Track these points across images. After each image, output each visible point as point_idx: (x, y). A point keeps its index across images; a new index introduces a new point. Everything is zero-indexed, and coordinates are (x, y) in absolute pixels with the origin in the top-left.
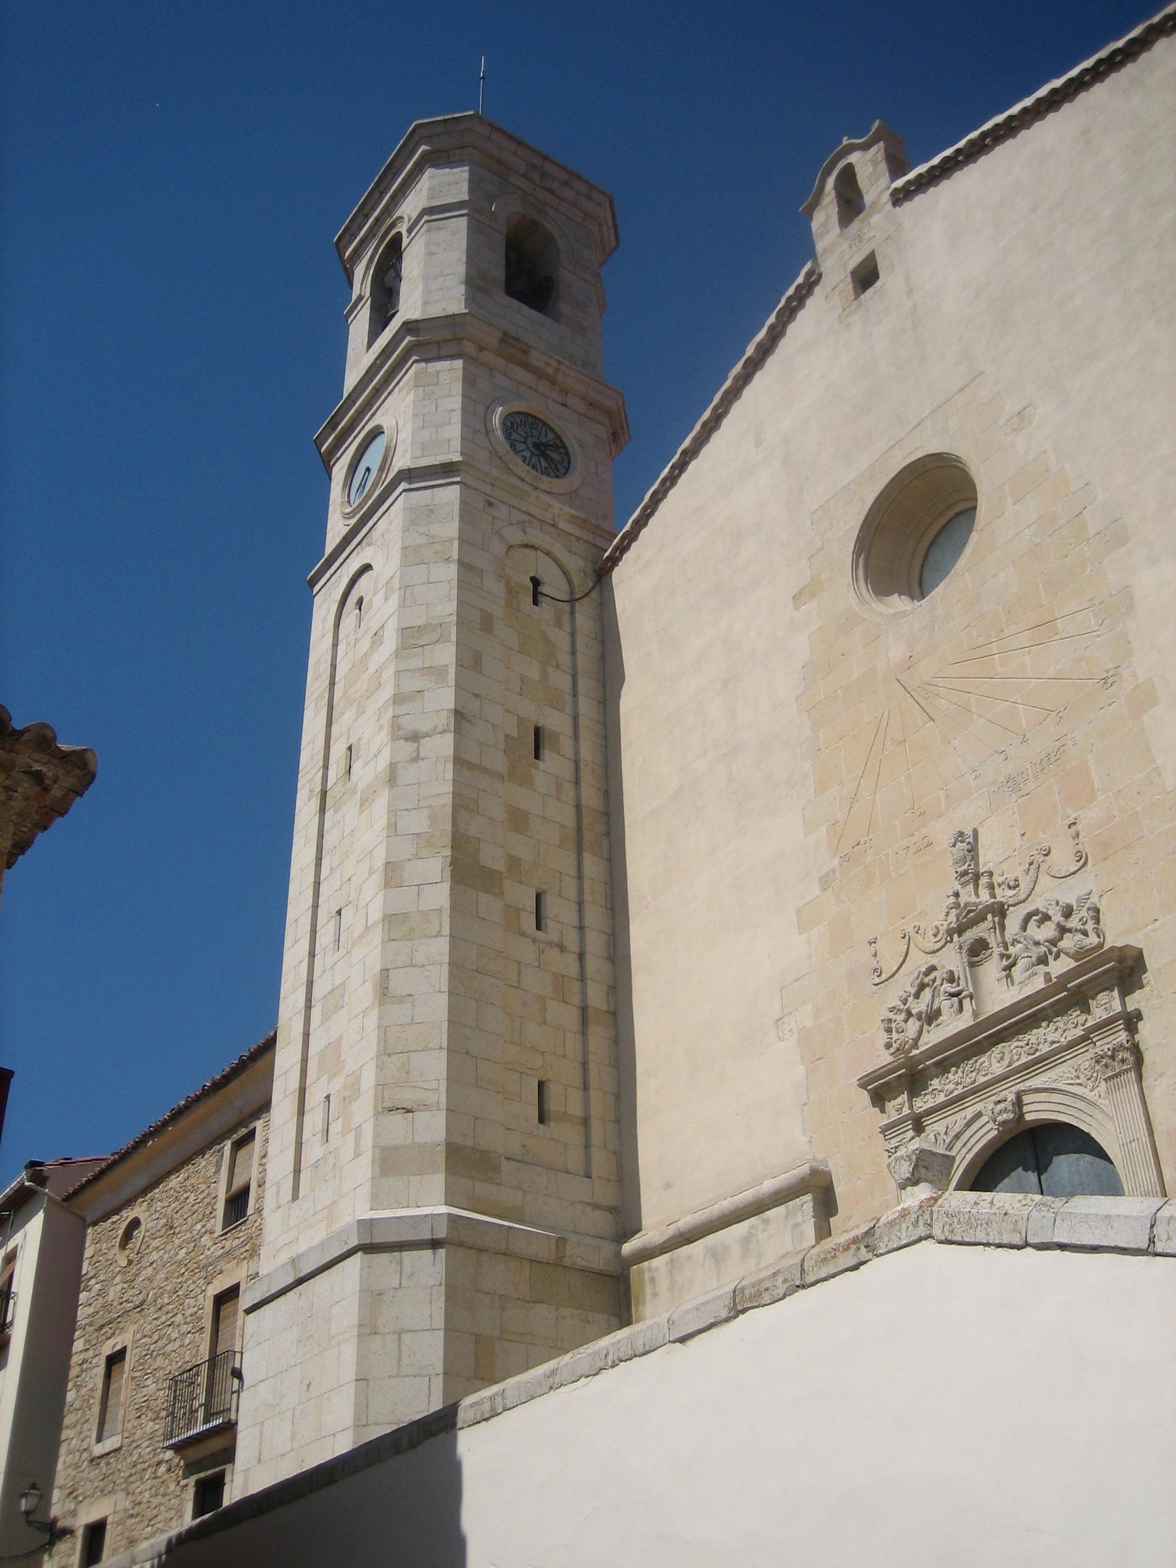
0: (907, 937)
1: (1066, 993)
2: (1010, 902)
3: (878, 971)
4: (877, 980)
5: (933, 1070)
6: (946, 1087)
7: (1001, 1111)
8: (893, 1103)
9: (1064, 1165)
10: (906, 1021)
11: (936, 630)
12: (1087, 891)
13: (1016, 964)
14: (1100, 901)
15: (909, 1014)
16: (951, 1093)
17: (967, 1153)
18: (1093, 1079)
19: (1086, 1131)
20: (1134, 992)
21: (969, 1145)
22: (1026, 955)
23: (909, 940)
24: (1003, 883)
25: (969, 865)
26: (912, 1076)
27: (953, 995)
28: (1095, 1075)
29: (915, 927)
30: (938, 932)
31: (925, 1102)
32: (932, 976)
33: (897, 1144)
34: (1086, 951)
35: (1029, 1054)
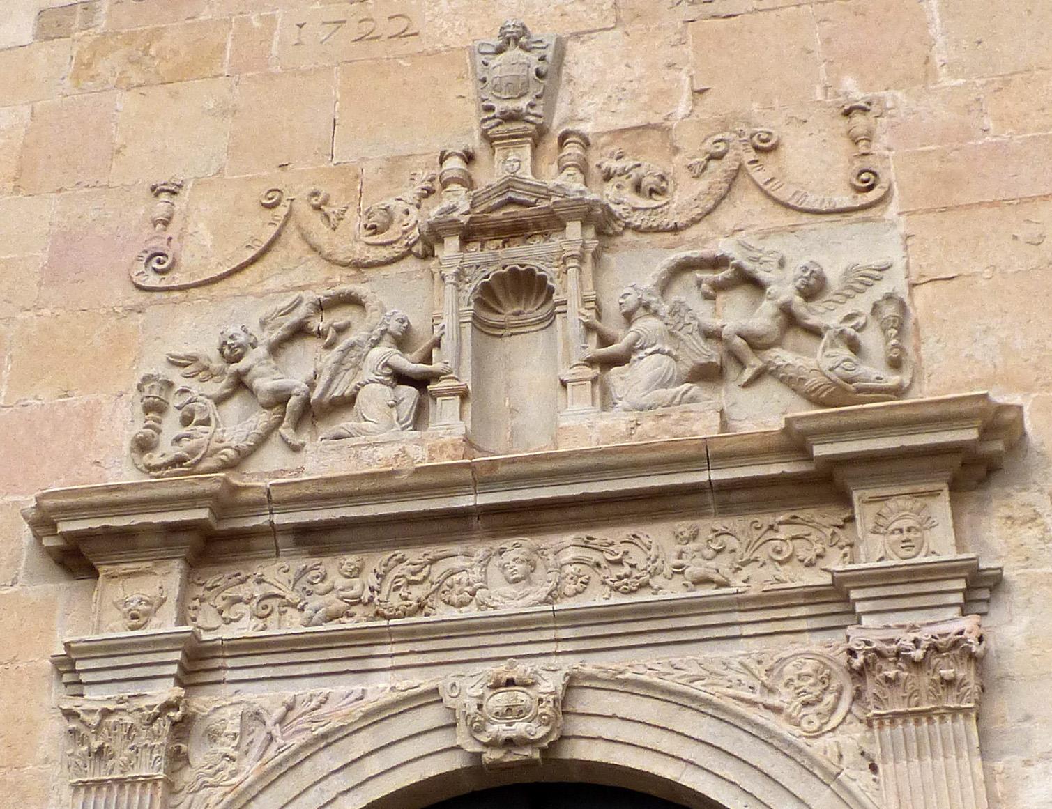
0: (282, 211)
2: (636, 220)
4: (153, 280)
6: (315, 602)
9: (67, 712)
10: (220, 400)
11: (163, 26)
12: (877, 262)
14: (910, 295)
15: (240, 384)
18: (819, 707)
22: (667, 349)
23: (288, 216)
25: (532, 106)
27: (400, 378)
28: (829, 698)
29: (315, 194)
30: (386, 227)
31: (228, 622)
32: (339, 317)
33: (111, 706)
34: (860, 390)
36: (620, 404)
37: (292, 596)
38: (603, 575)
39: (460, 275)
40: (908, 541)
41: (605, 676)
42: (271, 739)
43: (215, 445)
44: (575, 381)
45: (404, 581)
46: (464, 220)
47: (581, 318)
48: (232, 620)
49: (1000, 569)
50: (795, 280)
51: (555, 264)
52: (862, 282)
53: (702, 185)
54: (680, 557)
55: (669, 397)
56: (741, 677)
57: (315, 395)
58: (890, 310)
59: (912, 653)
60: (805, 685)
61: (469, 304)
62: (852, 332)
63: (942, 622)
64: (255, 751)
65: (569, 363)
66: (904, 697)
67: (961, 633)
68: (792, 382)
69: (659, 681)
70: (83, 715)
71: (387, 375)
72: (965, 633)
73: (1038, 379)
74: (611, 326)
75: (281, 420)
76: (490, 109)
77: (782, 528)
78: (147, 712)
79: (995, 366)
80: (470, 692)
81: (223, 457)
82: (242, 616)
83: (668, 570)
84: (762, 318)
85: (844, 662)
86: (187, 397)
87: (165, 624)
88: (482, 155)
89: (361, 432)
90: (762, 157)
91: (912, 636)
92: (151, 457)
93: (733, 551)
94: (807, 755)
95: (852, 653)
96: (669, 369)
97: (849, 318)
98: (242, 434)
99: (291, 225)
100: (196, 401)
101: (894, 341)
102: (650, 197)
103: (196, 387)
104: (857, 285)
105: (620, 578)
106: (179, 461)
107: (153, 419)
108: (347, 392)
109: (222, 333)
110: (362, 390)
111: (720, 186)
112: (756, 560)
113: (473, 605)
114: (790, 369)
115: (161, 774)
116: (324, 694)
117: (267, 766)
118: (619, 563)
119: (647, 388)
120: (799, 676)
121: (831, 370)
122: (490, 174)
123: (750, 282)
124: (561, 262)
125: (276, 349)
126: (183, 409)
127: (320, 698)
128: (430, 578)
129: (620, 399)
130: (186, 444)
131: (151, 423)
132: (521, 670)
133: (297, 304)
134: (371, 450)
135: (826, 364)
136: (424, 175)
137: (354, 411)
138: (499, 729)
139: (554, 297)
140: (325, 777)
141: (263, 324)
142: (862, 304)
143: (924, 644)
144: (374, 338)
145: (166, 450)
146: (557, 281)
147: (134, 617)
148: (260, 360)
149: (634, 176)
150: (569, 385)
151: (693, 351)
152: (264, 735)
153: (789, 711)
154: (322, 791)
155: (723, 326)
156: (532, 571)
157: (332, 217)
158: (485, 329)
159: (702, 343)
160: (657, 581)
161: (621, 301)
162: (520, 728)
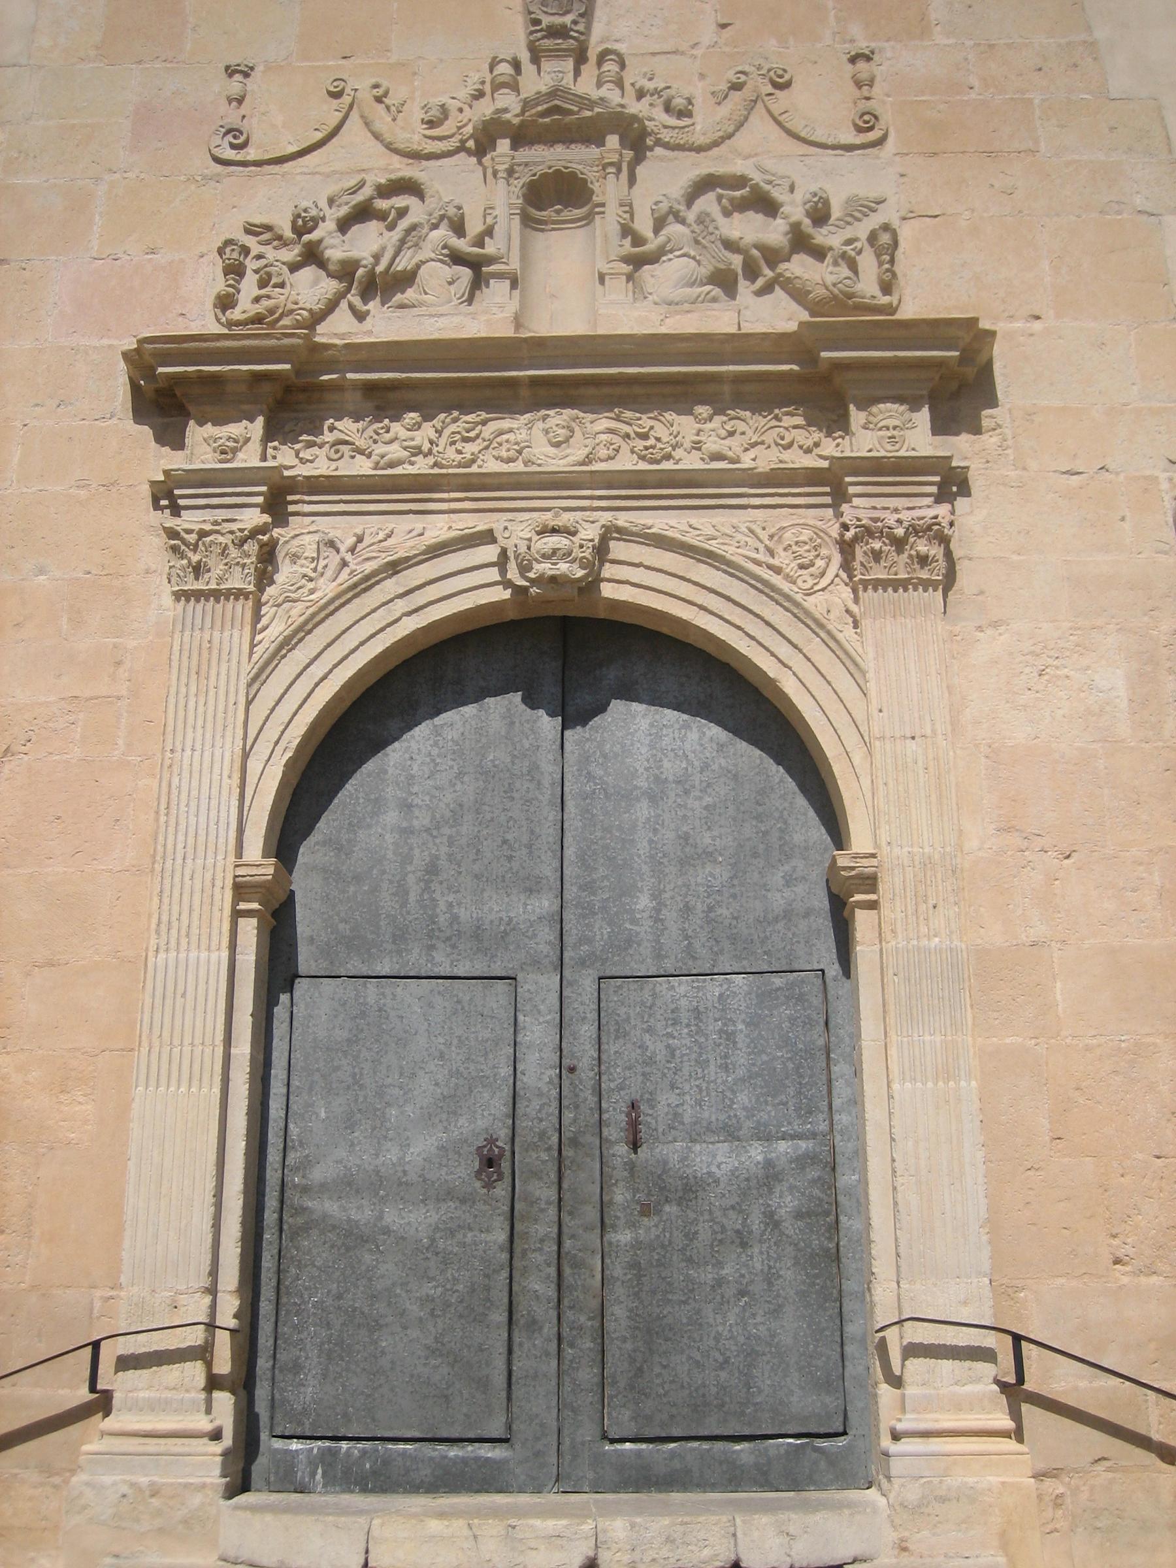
0: (346, 99)
1: (795, 367)
2: (666, 136)
3: (237, 137)
4: (230, 154)
5: (353, 399)
6: (380, 449)
7: (555, 551)
8: (209, 429)
10: (294, 267)
12: (873, 195)
13: (657, 261)
15: (313, 256)
16: (391, 465)
17: (409, 614)
19: (771, 675)
20: (957, 434)
21: (419, 598)
23: (351, 106)
24: (657, 92)
25: (575, 22)
26: (288, 389)
27: (457, 258)
29: (376, 86)
31: (303, 461)
32: (400, 201)
35: (643, 458)
36: (650, 297)
37: (361, 443)
38: (632, 444)
39: (510, 172)
40: (894, 437)
41: (634, 529)
42: (344, 564)
43: (291, 306)
44: (612, 274)
45: (458, 437)
46: (516, 121)
47: (620, 220)
48: (308, 461)
49: (968, 468)
50: (805, 204)
51: (595, 169)
52: (860, 211)
53: (724, 110)
54: (698, 435)
55: (695, 296)
56: (747, 539)
57: (380, 269)
58: (885, 238)
59: (895, 531)
60: (802, 550)
61: (518, 197)
62: (853, 254)
63: (920, 508)
64: (329, 573)
65: (607, 258)
66: (885, 567)
67: (936, 517)
68: (799, 294)
69: (680, 536)
70: (183, 534)
71: (446, 256)
72: (939, 518)
73: (1004, 311)
74: (644, 226)
75: (348, 290)
76: (537, 22)
77: (785, 418)
78: (239, 534)
79: (969, 296)
80: (521, 534)
81: (298, 317)
82: (317, 457)
83: (688, 445)
84: (775, 232)
85: (835, 534)
86: (263, 262)
87: (249, 458)
88: (528, 68)
89: (421, 304)
90: (777, 92)
91: (897, 516)
92: (232, 313)
93: (743, 433)
94: (803, 609)
95: (845, 527)
96: (694, 271)
97: (849, 242)
98: (315, 298)
99: (355, 115)
100: (271, 265)
101: (887, 266)
102: (679, 118)
103: (271, 253)
104: (857, 214)
105: (646, 448)
106: (258, 319)
107: (234, 279)
108: (409, 268)
109: (296, 207)
110: (423, 267)
111: (739, 113)
112: (762, 443)
113: (520, 462)
114: (797, 281)
115: (251, 588)
116: (390, 529)
117: (343, 586)
118: (645, 437)
119: (675, 286)
120: (797, 543)
121: (834, 285)
122: (534, 82)
123: (766, 205)
124: (600, 168)
125: (344, 226)
126: (262, 272)
127: (386, 532)
128: (482, 436)
129: (650, 294)
130: (266, 303)
131: (231, 282)
132: (566, 519)
133: (361, 185)
134: (433, 320)
135: (830, 279)
136: (475, 77)
137: (415, 286)
138: (544, 568)
139: (594, 198)
140: (391, 600)
141: (331, 202)
142: (862, 230)
143: (906, 524)
144: (434, 221)
145: (245, 307)
146: (597, 184)
147: (223, 452)
148: (331, 233)
149: (665, 97)
150: (607, 278)
151: (714, 257)
152: (337, 559)
153: (788, 571)
154: (390, 611)
155: (741, 238)
156: (571, 437)
157: (393, 109)
158: (528, 222)
159: (723, 250)
160: (679, 453)
161: (654, 207)
162: (563, 567)
